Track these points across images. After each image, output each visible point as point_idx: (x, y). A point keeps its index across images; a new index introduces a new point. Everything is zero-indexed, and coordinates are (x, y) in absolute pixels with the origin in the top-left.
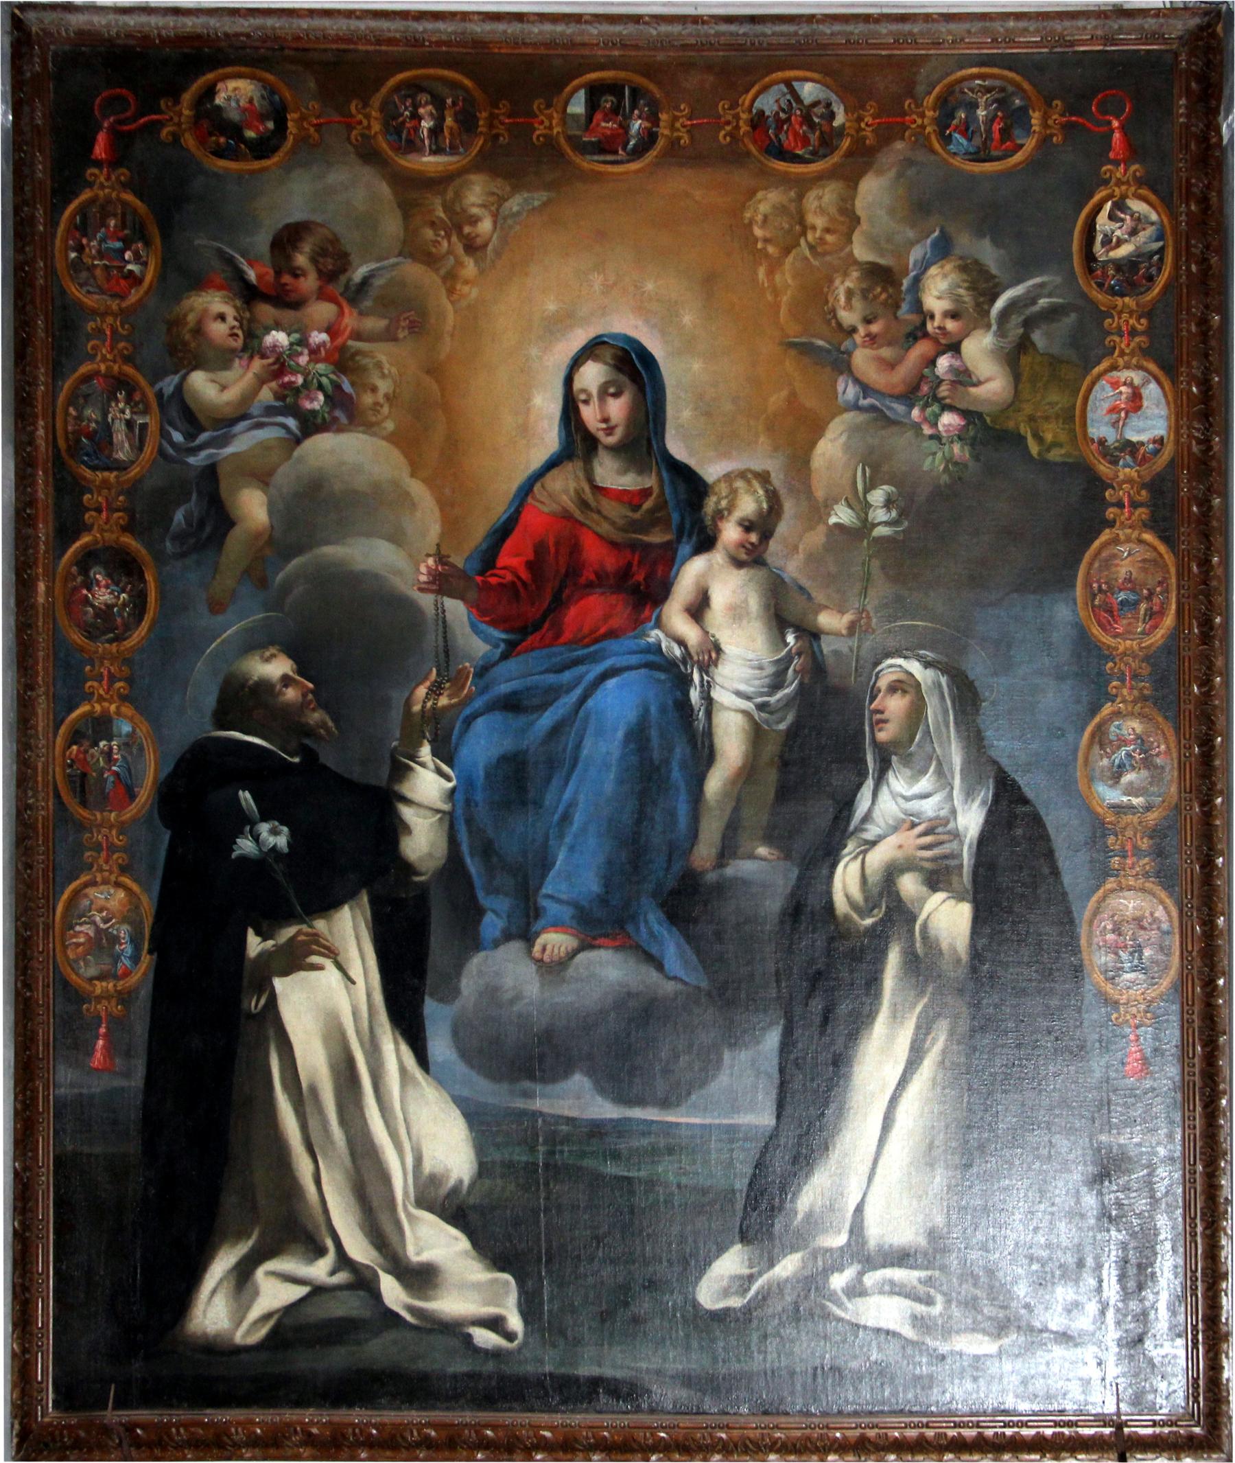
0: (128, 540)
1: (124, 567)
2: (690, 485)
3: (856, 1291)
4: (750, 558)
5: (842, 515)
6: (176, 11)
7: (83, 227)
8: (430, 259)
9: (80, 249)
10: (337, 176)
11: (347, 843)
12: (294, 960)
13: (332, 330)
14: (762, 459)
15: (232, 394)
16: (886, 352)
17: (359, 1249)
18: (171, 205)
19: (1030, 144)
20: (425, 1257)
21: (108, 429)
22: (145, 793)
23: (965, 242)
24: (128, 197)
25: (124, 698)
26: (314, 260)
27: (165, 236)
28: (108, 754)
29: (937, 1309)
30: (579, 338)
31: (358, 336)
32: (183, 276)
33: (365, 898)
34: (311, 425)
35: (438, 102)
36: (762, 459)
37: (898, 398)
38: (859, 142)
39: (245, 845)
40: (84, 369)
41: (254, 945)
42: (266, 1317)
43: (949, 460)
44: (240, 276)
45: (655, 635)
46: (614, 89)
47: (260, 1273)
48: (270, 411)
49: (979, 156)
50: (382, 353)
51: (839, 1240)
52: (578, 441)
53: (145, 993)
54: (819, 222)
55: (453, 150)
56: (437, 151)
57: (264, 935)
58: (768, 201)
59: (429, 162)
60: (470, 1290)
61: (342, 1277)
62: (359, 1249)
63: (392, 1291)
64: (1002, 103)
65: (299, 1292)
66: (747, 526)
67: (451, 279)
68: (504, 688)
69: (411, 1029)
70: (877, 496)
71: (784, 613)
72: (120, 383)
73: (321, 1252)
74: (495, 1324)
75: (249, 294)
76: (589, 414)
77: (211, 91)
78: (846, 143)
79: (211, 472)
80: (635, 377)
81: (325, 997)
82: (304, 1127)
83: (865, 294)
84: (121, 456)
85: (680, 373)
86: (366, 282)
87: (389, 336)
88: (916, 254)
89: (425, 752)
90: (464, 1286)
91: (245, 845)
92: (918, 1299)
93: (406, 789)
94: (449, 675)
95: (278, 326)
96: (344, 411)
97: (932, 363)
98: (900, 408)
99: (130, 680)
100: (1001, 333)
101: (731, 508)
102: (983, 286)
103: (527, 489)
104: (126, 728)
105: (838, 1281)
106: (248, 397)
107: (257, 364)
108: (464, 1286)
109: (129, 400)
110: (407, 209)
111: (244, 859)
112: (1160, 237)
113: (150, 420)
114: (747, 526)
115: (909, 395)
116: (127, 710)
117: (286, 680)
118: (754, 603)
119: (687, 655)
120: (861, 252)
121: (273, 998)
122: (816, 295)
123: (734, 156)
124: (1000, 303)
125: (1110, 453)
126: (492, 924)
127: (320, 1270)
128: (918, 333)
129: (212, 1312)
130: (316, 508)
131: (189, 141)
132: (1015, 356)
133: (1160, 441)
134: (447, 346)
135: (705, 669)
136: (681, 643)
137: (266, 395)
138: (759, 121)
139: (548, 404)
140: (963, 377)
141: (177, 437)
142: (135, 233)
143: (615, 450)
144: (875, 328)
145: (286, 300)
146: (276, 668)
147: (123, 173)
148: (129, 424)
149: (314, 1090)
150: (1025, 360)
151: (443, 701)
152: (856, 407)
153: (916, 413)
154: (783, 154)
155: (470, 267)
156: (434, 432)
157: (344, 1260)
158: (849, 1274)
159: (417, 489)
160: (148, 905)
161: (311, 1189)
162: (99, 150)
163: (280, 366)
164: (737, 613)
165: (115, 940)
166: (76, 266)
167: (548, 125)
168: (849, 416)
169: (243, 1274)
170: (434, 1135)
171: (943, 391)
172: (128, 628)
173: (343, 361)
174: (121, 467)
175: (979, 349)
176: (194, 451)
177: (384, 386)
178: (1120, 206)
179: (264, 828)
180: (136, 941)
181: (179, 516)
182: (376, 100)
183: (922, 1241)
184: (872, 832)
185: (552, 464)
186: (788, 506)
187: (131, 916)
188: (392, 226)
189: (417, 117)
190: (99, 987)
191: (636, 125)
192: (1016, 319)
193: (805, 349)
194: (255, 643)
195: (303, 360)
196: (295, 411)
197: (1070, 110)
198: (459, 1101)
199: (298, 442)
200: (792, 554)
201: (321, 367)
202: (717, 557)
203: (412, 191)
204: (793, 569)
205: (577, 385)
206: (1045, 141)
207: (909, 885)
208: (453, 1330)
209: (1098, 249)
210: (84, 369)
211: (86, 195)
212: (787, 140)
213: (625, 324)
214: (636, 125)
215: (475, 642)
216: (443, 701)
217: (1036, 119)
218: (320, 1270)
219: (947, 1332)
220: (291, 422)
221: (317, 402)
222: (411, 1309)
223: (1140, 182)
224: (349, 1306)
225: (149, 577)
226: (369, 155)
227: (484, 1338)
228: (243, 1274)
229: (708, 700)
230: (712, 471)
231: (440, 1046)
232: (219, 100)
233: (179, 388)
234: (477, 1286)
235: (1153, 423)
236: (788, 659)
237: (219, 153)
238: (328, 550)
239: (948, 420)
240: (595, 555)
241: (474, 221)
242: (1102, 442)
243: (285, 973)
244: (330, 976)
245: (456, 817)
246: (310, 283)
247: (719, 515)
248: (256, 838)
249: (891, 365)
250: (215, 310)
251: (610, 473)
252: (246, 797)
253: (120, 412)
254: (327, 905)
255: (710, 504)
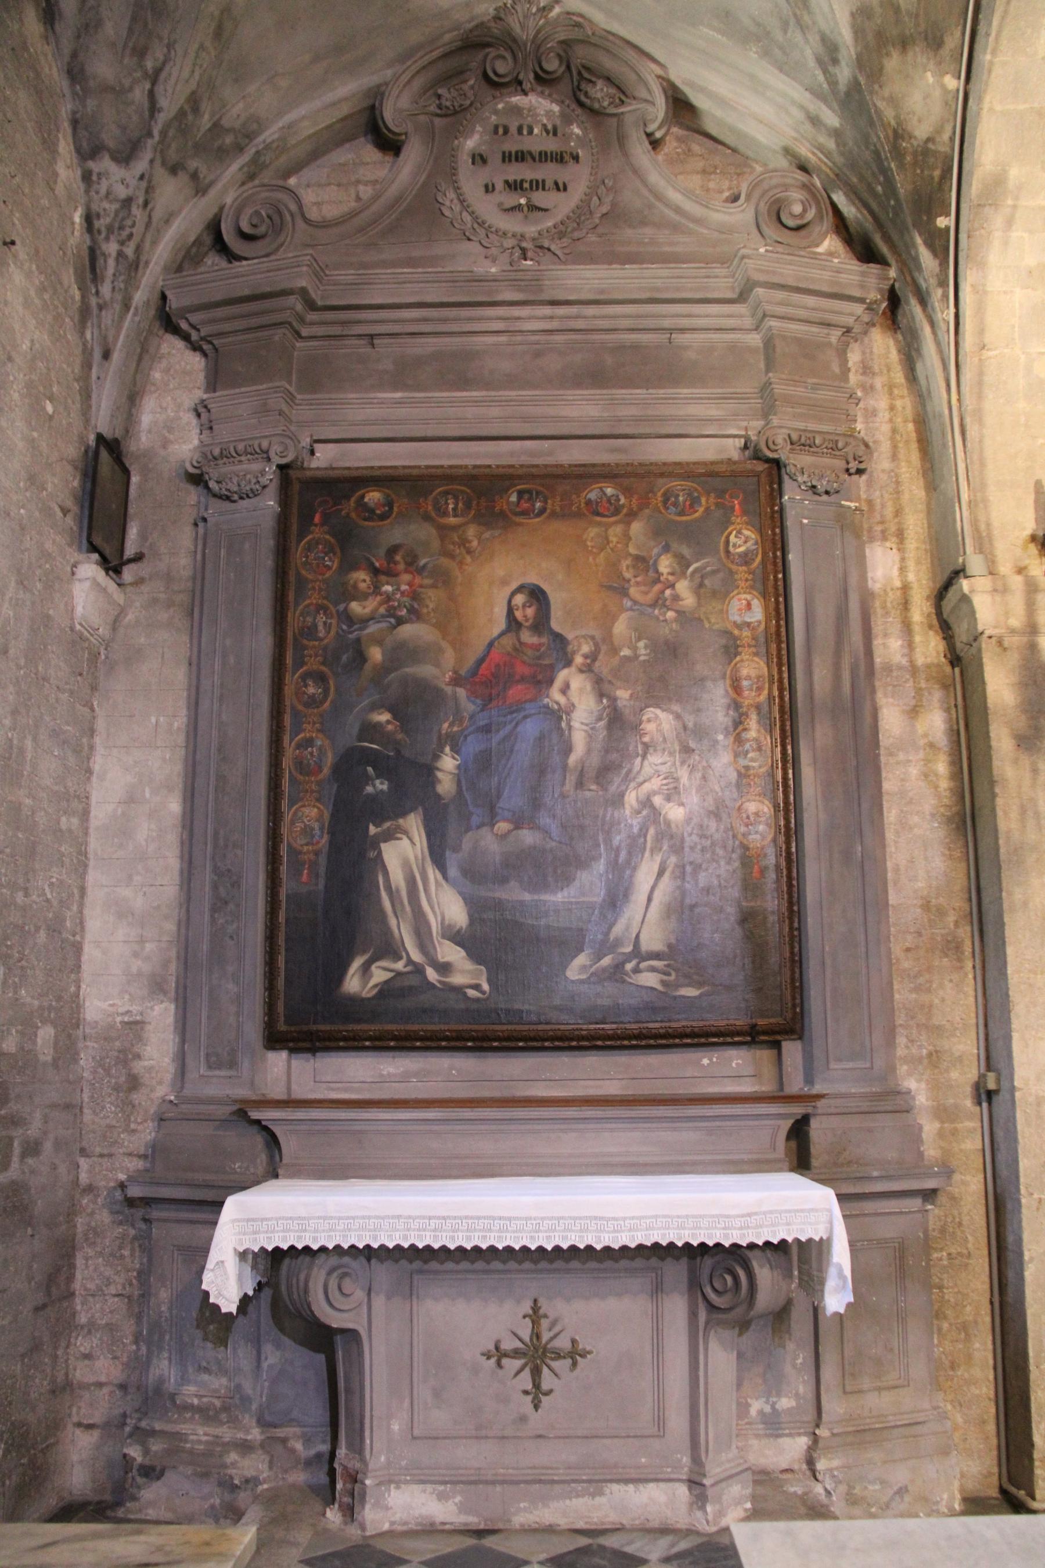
0: (323, 668)
1: (321, 679)
2: (560, 639)
3: (636, 970)
4: (587, 669)
5: (626, 652)
6: (349, 468)
7: (309, 548)
8: (452, 556)
9: (307, 557)
10: (412, 527)
11: (411, 783)
12: (389, 836)
13: (410, 584)
14: (592, 630)
15: (367, 610)
16: (643, 588)
17: (416, 956)
18: (347, 541)
19: (701, 510)
20: (445, 960)
21: (316, 626)
22: (326, 771)
23: (675, 546)
24: (328, 537)
25: (319, 731)
26: (403, 558)
27: (342, 550)
28: (311, 754)
29: (673, 977)
30: (514, 586)
31: (421, 586)
32: (349, 565)
33: (420, 809)
34: (400, 621)
35: (456, 498)
36: (592, 630)
37: (650, 606)
38: (631, 509)
39: (369, 789)
40: (307, 602)
41: (373, 830)
42: (376, 986)
43: (671, 630)
44: (372, 564)
45: (546, 700)
46: (529, 492)
47: (373, 968)
48: (383, 616)
49: (682, 513)
50: (431, 593)
51: (628, 949)
52: (513, 623)
53: (325, 850)
54: (615, 540)
55: (462, 515)
56: (455, 516)
57: (377, 826)
58: (593, 532)
59: (452, 520)
60: (465, 972)
61: (409, 968)
62: (416, 956)
63: (431, 975)
64: (689, 495)
65: (390, 975)
66: (586, 657)
67: (461, 563)
68: (482, 723)
69: (439, 863)
70: (641, 644)
71: (601, 689)
72: (320, 608)
73: (400, 958)
74: (477, 987)
75: (376, 572)
76: (518, 614)
77: (363, 497)
78: (625, 511)
79: (358, 640)
80: (538, 600)
81: (403, 852)
82: (393, 905)
83: (634, 567)
84: (321, 635)
85: (556, 599)
86: (424, 566)
87: (434, 586)
88: (655, 551)
89: (447, 749)
90: (463, 972)
91: (369, 789)
92: (665, 974)
93: (439, 764)
94: (458, 718)
95: (388, 583)
96: (414, 614)
97: (663, 592)
98: (650, 610)
99: (322, 723)
100: (691, 580)
101: (578, 650)
102: (683, 563)
103: (491, 645)
104: (319, 743)
105: (629, 966)
106: (376, 609)
107: (379, 598)
108: (463, 972)
109: (325, 614)
110: (442, 538)
111: (369, 795)
112: (756, 543)
113: (334, 621)
114: (586, 657)
115: (654, 605)
116: (320, 735)
117: (388, 722)
118: (589, 687)
119: (560, 709)
120: (632, 550)
121: (380, 853)
122: (613, 566)
123: (579, 515)
124: (691, 569)
125: (739, 626)
126: (475, 820)
127: (400, 966)
128: (657, 581)
129: (353, 984)
130: (402, 654)
131: (353, 515)
132: (698, 589)
133: (760, 622)
134: (458, 590)
135: (568, 714)
136: (557, 703)
137: (382, 610)
138: (589, 502)
139: (500, 612)
140: (676, 598)
141: (344, 627)
142: (330, 550)
143: (530, 628)
144: (639, 579)
145: (391, 574)
146: (383, 717)
147: (326, 528)
148: (325, 623)
149: (398, 890)
150: (702, 590)
151: (455, 729)
152: (631, 609)
153: (656, 612)
154: (598, 514)
155: (468, 559)
156: (452, 622)
157: (410, 962)
158: (634, 963)
159: (444, 644)
160: (327, 815)
161: (396, 931)
162: (317, 519)
163: (389, 598)
164: (581, 690)
165: (312, 829)
166: (306, 563)
167: (501, 504)
168: (629, 613)
169: (366, 968)
170: (449, 907)
171: (668, 603)
172: (322, 702)
173: (415, 596)
174: (321, 640)
175: (683, 587)
176: (351, 633)
177: (431, 606)
178: (739, 532)
179: (377, 782)
180: (322, 829)
181: (345, 658)
182: (431, 498)
183: (666, 949)
184: (641, 779)
185: (502, 634)
186: (604, 648)
187: (320, 819)
188: (436, 544)
189: (447, 504)
190: (305, 848)
191: (538, 505)
192: (698, 575)
193: (610, 588)
194: (374, 707)
195: (398, 596)
196: (393, 616)
197: (718, 497)
198: (460, 893)
199: (395, 627)
200: (603, 666)
201: (405, 599)
202: (573, 669)
203: (444, 531)
204: (605, 672)
205: (513, 603)
206: (707, 509)
207: (657, 800)
208: (458, 990)
209: (731, 549)
210: (307, 602)
211: (310, 537)
212: (600, 510)
213: (532, 579)
214: (538, 505)
215: (469, 707)
216: (455, 729)
217: (703, 500)
218: (400, 966)
219: (677, 986)
220: (392, 620)
221: (404, 612)
222: (440, 982)
223: (747, 523)
224: (413, 981)
225: (331, 682)
226: (427, 518)
227: (472, 993)
228: (366, 968)
229: (570, 728)
230: (570, 636)
231: (453, 872)
232: (366, 500)
233: (346, 609)
234: (469, 972)
235: (757, 614)
236: (605, 708)
237: (365, 519)
238: (407, 670)
239: (670, 614)
240: (521, 670)
241: (470, 542)
242: (735, 622)
243: (385, 841)
244: (405, 842)
245: (462, 774)
246: (401, 567)
247: (574, 653)
248: (374, 786)
249: (646, 593)
250: (361, 578)
251: (527, 637)
252: (370, 769)
253: (321, 619)
254: (404, 814)
255: (570, 648)
